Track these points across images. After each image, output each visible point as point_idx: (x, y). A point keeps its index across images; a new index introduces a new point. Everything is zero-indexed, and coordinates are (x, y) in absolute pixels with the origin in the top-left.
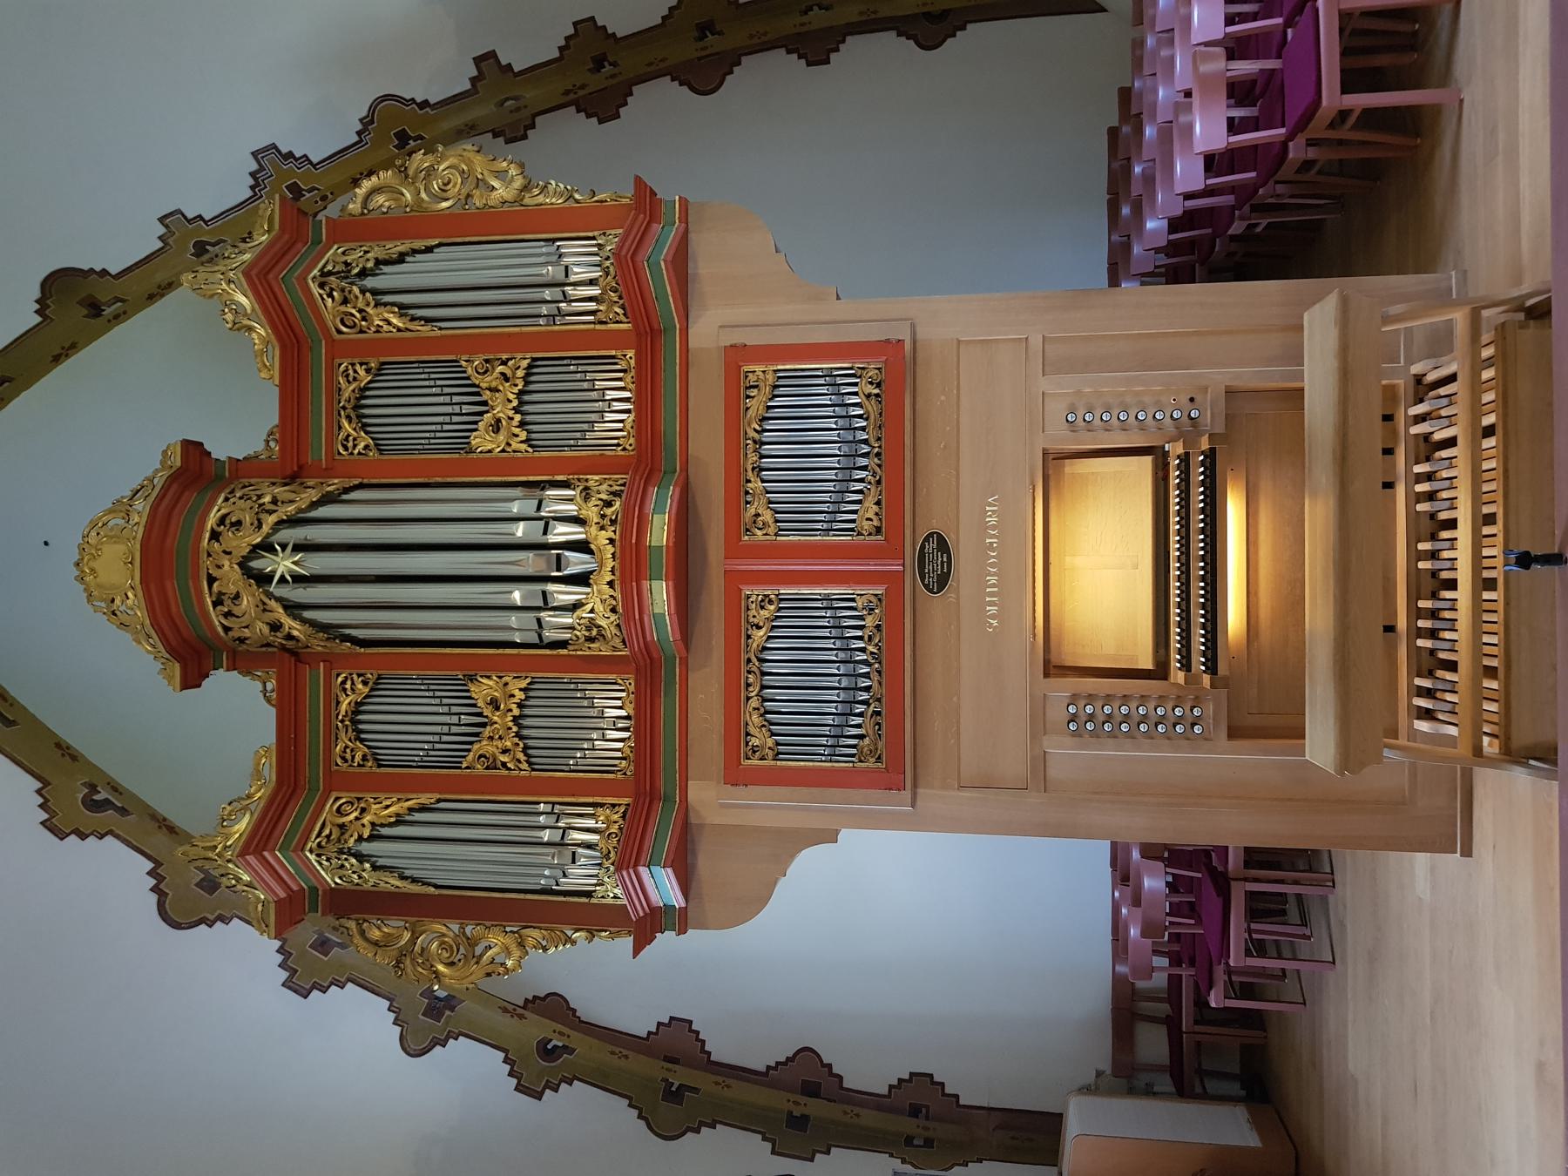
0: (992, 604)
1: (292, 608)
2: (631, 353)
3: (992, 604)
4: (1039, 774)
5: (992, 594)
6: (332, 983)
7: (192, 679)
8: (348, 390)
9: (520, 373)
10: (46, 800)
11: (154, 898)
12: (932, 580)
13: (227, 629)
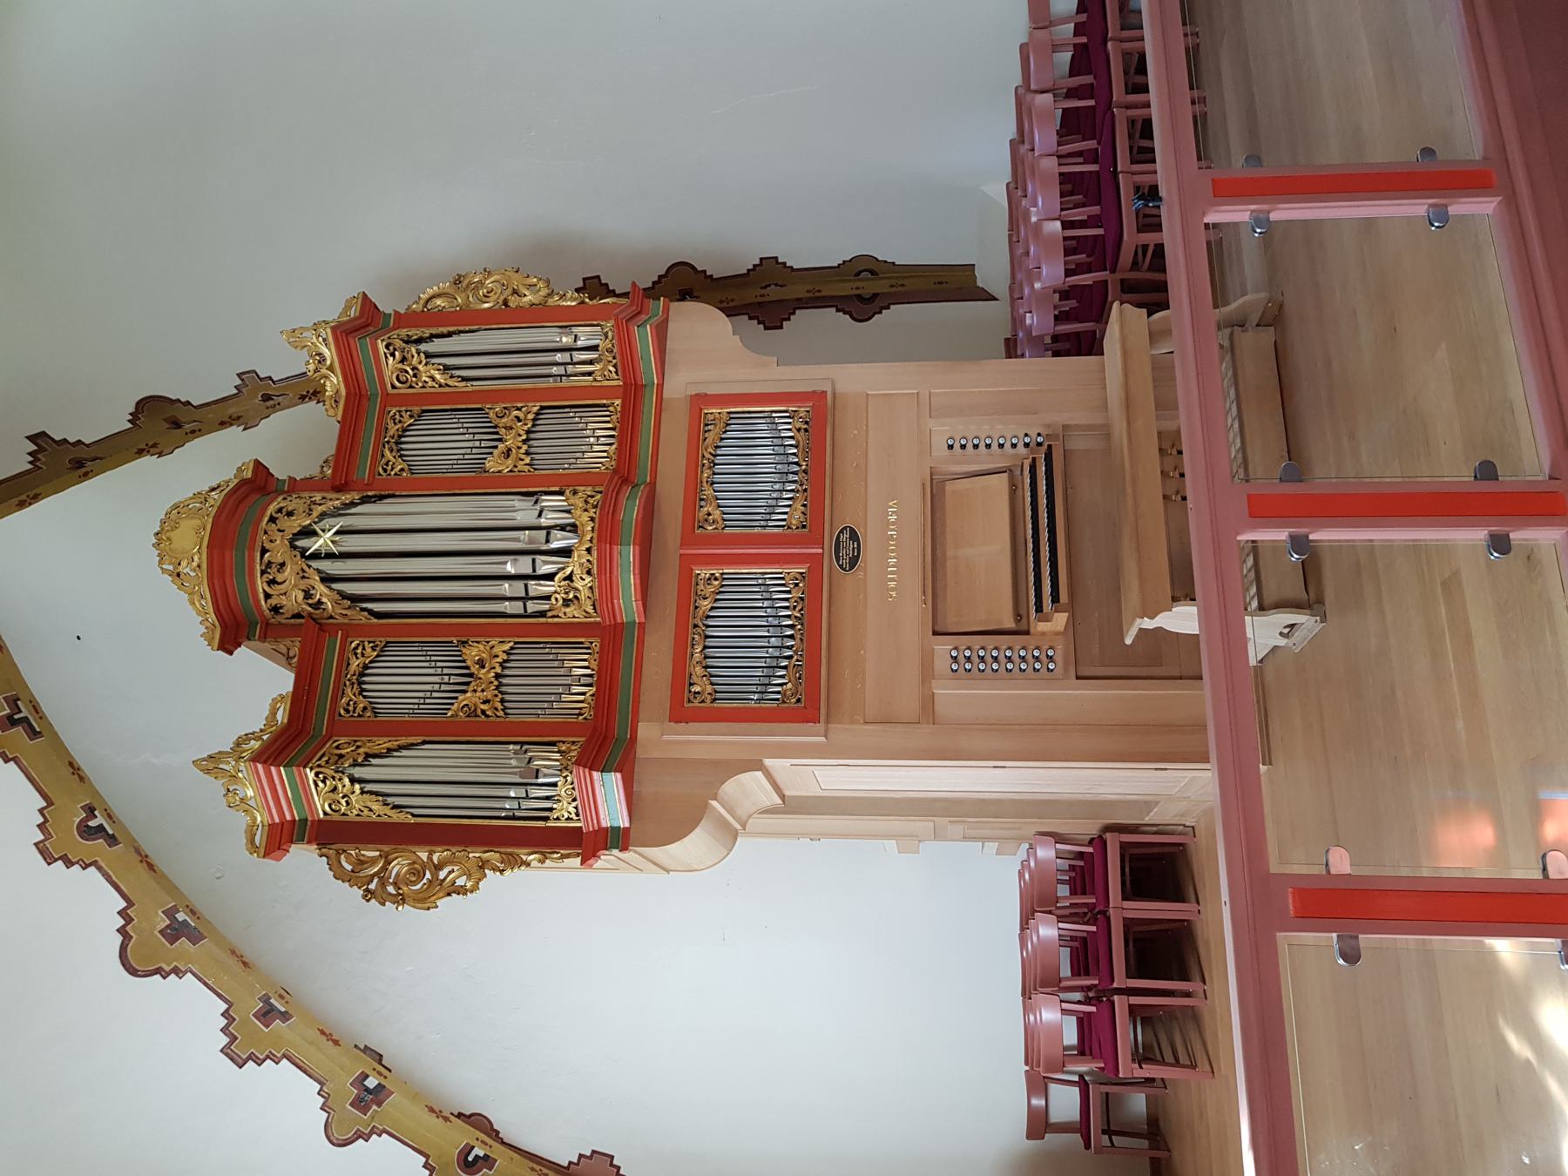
0: (892, 580)
1: (327, 579)
2: (618, 402)
3: (892, 580)
4: (928, 710)
5: (892, 573)
6: (268, 1057)
7: (228, 644)
8: (393, 429)
9: (531, 416)
10: (46, 820)
11: (119, 938)
12: (846, 562)
13: (267, 596)
